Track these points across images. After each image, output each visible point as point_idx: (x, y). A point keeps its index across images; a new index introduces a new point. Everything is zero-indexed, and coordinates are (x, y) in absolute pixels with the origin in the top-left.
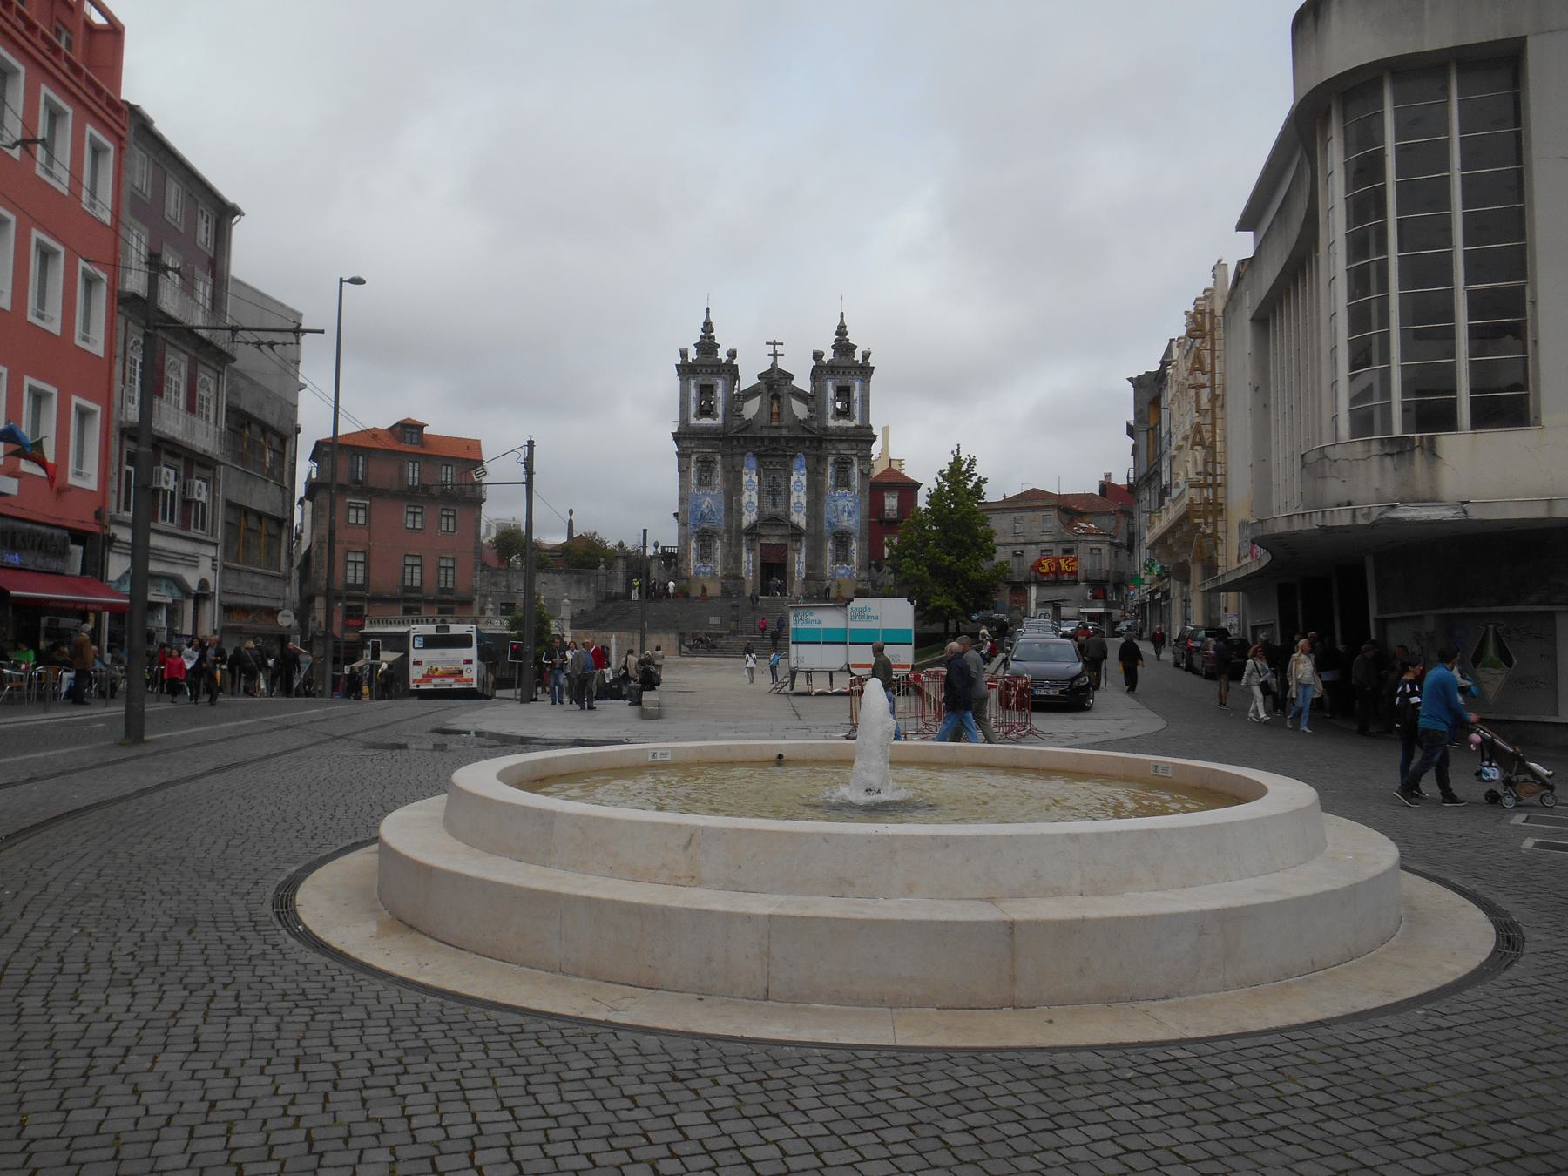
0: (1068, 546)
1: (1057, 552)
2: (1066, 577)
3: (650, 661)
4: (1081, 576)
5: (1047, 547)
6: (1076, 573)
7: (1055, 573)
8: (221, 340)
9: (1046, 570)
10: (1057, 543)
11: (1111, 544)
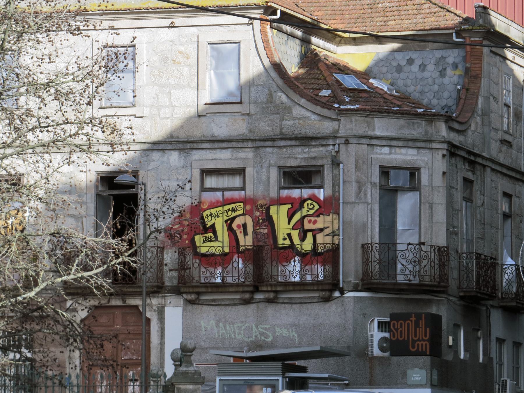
0: (299, 157)
1: (262, 178)
2: (294, 270)
3: (5, 355)
4: (350, 265)
5: (223, 158)
6: (331, 256)
7: (256, 256)
8: (4, 155)
9: (221, 244)
10: (259, 142)
11: (453, 151)
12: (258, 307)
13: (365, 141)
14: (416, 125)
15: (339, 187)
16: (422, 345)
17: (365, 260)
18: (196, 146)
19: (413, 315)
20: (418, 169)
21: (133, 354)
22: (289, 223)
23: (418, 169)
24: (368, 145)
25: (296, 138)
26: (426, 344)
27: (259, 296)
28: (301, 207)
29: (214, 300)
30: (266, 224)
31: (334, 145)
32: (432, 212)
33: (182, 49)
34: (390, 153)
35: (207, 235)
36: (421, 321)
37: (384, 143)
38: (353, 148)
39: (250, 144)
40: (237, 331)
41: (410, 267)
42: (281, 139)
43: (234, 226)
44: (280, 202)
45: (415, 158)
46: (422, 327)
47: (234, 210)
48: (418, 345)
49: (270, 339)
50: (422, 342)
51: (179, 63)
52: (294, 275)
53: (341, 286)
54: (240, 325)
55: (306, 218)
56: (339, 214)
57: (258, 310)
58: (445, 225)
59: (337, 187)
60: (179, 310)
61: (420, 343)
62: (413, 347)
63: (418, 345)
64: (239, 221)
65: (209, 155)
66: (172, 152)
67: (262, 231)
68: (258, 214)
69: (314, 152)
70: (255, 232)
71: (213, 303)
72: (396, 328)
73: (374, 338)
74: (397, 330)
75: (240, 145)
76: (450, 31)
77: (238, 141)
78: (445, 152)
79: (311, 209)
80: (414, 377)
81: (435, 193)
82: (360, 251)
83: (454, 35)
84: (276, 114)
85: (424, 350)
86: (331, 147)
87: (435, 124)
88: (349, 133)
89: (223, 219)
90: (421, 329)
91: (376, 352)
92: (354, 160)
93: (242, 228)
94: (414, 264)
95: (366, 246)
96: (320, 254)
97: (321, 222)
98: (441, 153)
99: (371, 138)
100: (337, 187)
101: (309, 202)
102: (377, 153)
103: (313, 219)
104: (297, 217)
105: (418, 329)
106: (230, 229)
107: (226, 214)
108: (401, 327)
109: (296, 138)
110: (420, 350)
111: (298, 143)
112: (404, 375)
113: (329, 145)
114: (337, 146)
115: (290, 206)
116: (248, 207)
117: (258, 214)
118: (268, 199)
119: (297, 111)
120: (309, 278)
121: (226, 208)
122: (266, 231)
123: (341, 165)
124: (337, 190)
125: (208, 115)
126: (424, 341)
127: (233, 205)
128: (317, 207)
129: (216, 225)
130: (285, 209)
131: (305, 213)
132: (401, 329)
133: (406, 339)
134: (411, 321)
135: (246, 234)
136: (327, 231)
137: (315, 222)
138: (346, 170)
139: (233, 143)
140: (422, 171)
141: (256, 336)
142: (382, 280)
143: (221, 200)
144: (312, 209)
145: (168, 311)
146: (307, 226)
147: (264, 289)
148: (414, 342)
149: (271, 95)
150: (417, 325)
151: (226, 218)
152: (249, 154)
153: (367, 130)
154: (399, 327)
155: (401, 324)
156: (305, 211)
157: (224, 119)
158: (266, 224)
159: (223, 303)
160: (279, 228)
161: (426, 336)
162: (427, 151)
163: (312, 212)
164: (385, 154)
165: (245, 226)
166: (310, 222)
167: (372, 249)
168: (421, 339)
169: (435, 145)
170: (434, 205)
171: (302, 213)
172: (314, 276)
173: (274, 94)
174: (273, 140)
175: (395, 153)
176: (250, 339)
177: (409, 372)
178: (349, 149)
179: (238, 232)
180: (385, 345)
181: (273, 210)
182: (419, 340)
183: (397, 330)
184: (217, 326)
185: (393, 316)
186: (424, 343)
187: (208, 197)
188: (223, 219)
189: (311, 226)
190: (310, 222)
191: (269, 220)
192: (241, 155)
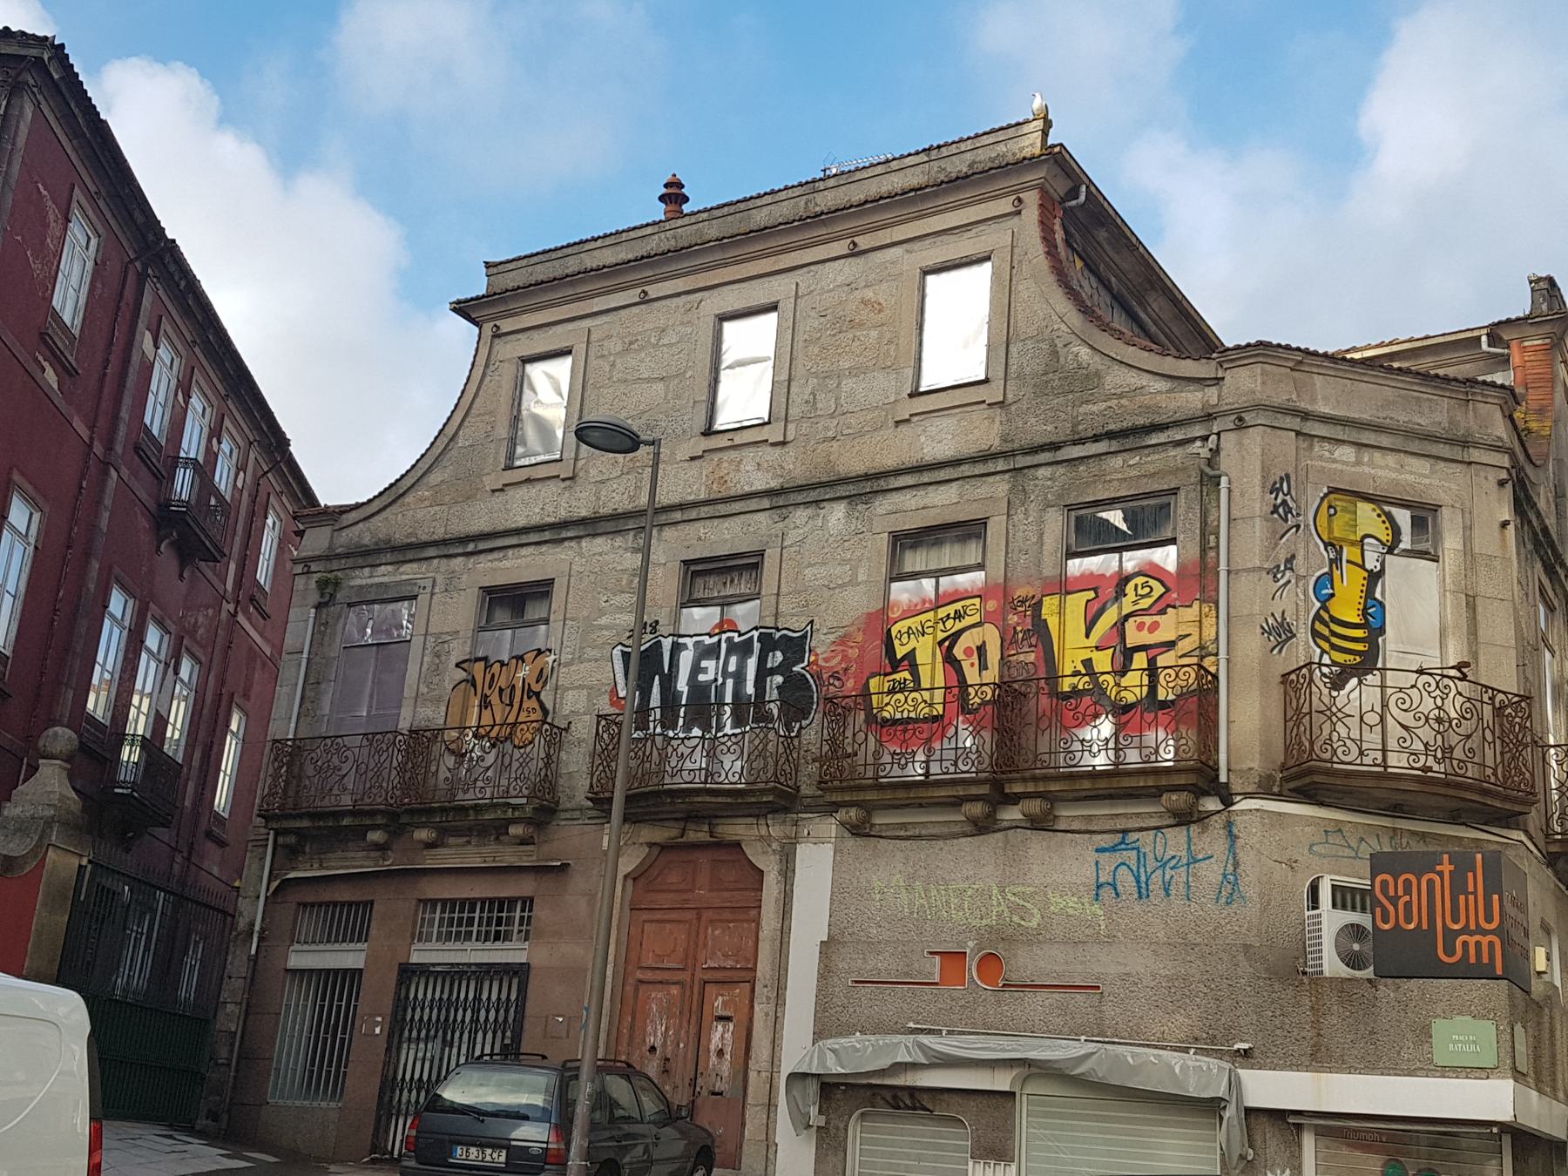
4: (1246, 727)
5: (942, 502)
12: (1007, 841)
13: (1289, 421)
14: (1426, 405)
15: (1217, 538)
16: (1478, 943)
17: (1290, 713)
18: (883, 484)
19: (1446, 857)
20: (1435, 509)
21: (726, 956)
22: (1087, 636)
23: (1435, 509)
24: (1298, 433)
25: (1110, 435)
26: (1491, 944)
27: (1012, 814)
28: (1120, 593)
29: (903, 826)
30: (1033, 641)
31: (1205, 438)
32: (1475, 618)
33: (869, 294)
34: (1358, 463)
35: (897, 676)
36: (1470, 875)
37: (1338, 433)
38: (1254, 440)
39: (1001, 465)
40: (954, 901)
41: (1426, 733)
42: (1075, 443)
43: (958, 652)
44: (1064, 587)
45: (1427, 481)
46: (1475, 893)
47: (958, 616)
48: (1465, 944)
49: (1034, 924)
50: (1478, 937)
51: (861, 324)
52: (1095, 749)
53: (1223, 778)
54: (961, 886)
55: (1131, 620)
56: (1217, 604)
57: (1005, 849)
58: (1513, 653)
59: (1212, 538)
60: (828, 850)
61: (1472, 940)
62: (1450, 951)
63: (1465, 944)
64: (968, 641)
65: (908, 500)
66: (835, 505)
67: (1021, 658)
68: (1013, 619)
69: (1152, 462)
70: (1004, 661)
71: (902, 833)
72: (1392, 893)
73: (1324, 926)
74: (1394, 900)
75: (979, 469)
76: (1476, 334)
77: (973, 460)
78: (1504, 475)
79: (1143, 597)
80: (1455, 1042)
81: (1482, 571)
82: (1277, 693)
83: (1484, 338)
84: (1065, 394)
85: (1485, 960)
86: (1198, 443)
87: (1474, 409)
88: (1242, 402)
89: (935, 637)
90: (1471, 897)
91: (1331, 964)
92: (1258, 465)
93: (976, 655)
94: (1436, 726)
95: (1293, 677)
96: (1164, 705)
97: (1167, 628)
98: (1494, 476)
99: (1306, 416)
100: (1212, 538)
101: (1140, 580)
102: (1321, 458)
103: (1148, 620)
104: (1110, 617)
105: (1462, 898)
106: (950, 660)
107: (941, 626)
108: (1408, 891)
109: (1110, 435)
110: (1473, 960)
111: (1115, 445)
112: (1425, 1034)
113: (1192, 440)
114: (1214, 437)
115: (1092, 594)
116: (992, 605)
117: (1013, 619)
118: (1037, 583)
119: (1119, 379)
120: (1132, 757)
121: (942, 612)
122: (1032, 657)
123: (1224, 480)
124: (1212, 544)
125: (915, 419)
126: (1485, 933)
127: (958, 606)
128: (1159, 589)
129: (917, 653)
130: (1077, 603)
131: (1127, 605)
132: (1407, 898)
133: (1425, 927)
134: (1441, 874)
135: (983, 666)
136: (1185, 646)
137: (1154, 627)
138: (1236, 493)
139: (964, 468)
140: (1445, 513)
141: (999, 915)
142: (1343, 763)
143: (933, 596)
144: (1148, 595)
145: (803, 851)
146: (1133, 637)
147: (1018, 788)
148: (1450, 936)
149: (1055, 353)
150: (1458, 887)
151: (941, 636)
152: (1000, 487)
153: (1294, 397)
154: (1400, 893)
155: (1407, 883)
156: (1127, 605)
157: (946, 423)
158: (1033, 641)
159: (924, 832)
160: (1062, 648)
161: (1489, 919)
162: (1458, 468)
163: (1146, 603)
164: (1345, 463)
165: (981, 649)
166: (1140, 627)
167: (1311, 680)
168: (1473, 927)
169: (1476, 455)
170: (1479, 601)
171: (1120, 608)
172: (1146, 752)
173: (1062, 352)
174: (1054, 447)
175: (1371, 464)
176: (984, 922)
177: (1439, 1027)
178: (1246, 442)
179: (965, 665)
180: (1356, 947)
181: (1049, 606)
182: (1465, 930)
183: (1394, 900)
184: (909, 888)
185: (1378, 864)
186: (1485, 940)
187: (902, 592)
188: (935, 637)
189: (1146, 638)
190: (1140, 627)
191: (1040, 629)
192: (983, 489)
